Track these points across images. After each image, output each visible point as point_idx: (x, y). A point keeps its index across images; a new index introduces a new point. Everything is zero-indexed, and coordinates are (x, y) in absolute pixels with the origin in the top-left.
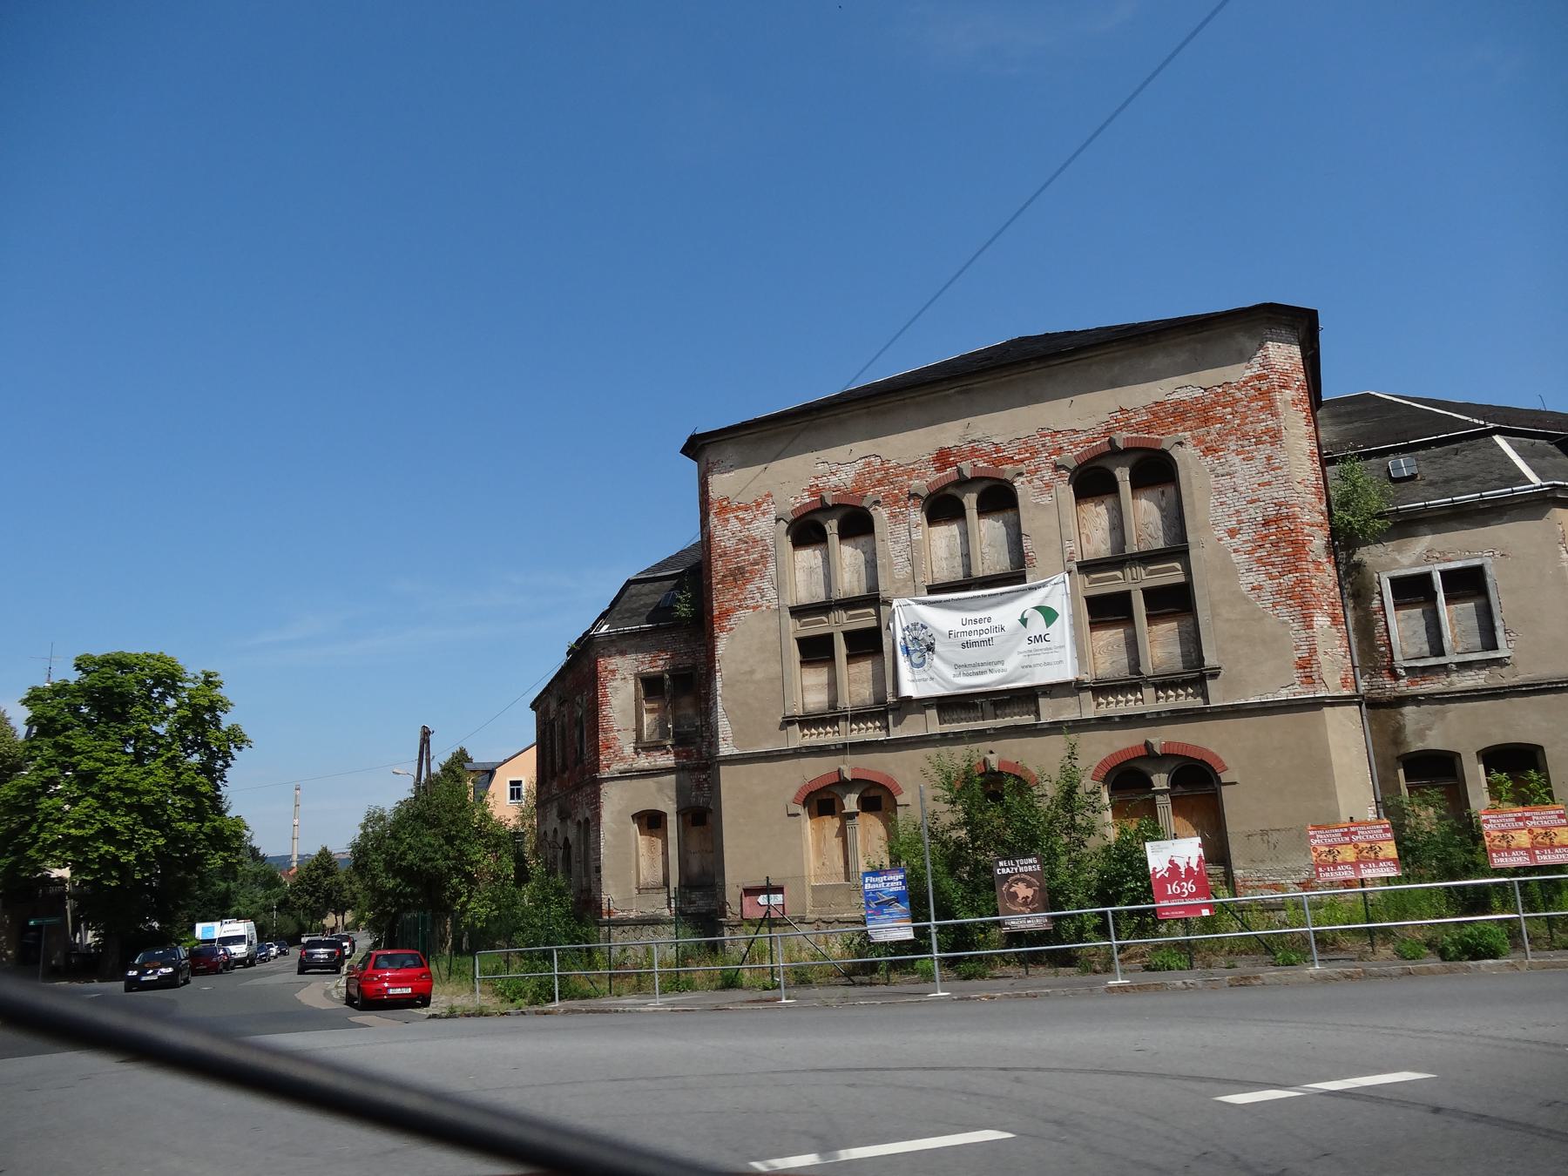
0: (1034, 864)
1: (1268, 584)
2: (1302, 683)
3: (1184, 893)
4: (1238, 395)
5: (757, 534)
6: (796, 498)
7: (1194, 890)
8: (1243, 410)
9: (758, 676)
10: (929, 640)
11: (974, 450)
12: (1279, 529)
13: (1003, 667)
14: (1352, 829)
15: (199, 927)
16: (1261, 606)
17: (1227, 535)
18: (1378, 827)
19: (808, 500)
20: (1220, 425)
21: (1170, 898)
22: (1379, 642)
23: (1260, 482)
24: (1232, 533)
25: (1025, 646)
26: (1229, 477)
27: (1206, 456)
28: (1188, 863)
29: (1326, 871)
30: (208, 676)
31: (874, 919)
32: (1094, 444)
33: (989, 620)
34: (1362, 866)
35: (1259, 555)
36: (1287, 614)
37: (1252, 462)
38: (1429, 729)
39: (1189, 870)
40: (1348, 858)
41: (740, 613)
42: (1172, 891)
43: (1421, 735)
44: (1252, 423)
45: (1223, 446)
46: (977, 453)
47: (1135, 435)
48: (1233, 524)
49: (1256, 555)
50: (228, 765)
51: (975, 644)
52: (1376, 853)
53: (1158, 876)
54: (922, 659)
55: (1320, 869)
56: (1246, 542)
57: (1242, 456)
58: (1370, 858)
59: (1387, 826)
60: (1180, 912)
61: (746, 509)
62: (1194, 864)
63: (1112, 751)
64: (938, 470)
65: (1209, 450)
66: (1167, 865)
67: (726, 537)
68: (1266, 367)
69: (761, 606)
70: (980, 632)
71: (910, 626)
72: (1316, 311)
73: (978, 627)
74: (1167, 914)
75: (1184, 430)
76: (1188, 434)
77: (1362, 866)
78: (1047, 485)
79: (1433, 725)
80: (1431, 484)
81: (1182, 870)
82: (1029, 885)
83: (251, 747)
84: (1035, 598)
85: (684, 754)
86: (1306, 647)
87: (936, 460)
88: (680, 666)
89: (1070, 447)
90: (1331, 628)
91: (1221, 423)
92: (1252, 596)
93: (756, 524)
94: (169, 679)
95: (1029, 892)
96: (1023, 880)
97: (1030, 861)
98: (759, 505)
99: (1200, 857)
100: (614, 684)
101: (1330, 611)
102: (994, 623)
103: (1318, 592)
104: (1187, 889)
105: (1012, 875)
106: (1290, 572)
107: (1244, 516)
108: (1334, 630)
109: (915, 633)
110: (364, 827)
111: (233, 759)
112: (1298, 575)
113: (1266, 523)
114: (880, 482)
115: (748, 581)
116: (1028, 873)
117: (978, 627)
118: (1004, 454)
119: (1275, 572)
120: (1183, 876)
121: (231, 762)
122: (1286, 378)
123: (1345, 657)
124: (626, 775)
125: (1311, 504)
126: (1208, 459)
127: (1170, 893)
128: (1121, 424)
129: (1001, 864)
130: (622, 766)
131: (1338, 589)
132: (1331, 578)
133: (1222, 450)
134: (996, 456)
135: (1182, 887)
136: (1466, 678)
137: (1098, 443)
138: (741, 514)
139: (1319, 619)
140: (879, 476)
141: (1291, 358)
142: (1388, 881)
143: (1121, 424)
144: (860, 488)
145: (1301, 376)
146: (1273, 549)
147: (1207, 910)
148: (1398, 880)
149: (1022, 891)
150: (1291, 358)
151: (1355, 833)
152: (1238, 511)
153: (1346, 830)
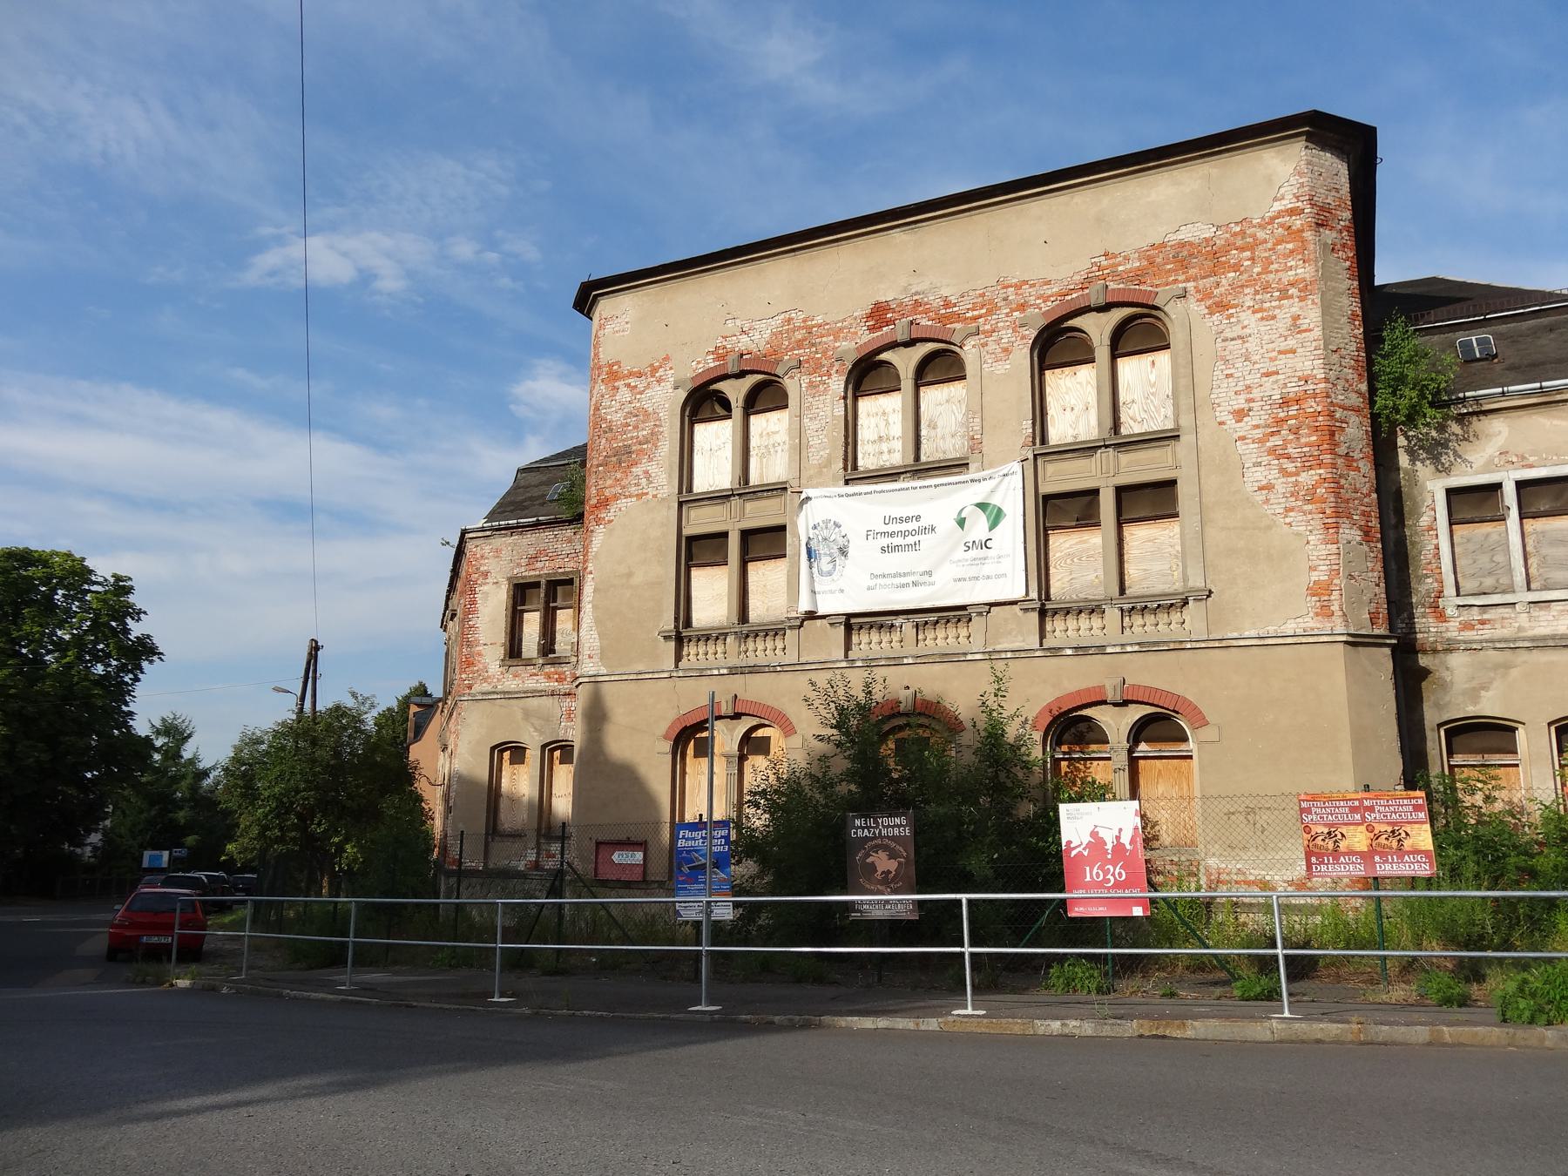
0: (901, 825)
1: (1282, 486)
2: (1317, 614)
3: (1109, 881)
4: (1261, 235)
5: (649, 406)
6: (699, 363)
7: (1124, 877)
8: (1266, 255)
9: (638, 579)
10: (841, 542)
11: (917, 303)
12: (1301, 411)
13: (931, 579)
14: (1367, 803)
15: (147, 854)
16: (1269, 512)
17: (1231, 417)
18: (1405, 802)
19: (712, 365)
20: (1233, 274)
21: (1087, 887)
22: (1425, 572)
23: (1282, 348)
24: (1240, 415)
25: (960, 553)
26: (1240, 341)
27: (1211, 314)
28: (1118, 838)
29: (1323, 863)
30: (118, 578)
31: (685, 889)
32: (1069, 298)
33: (918, 518)
34: (1377, 858)
35: (1272, 444)
36: (1304, 523)
37: (1272, 322)
38: (1484, 688)
39: (1118, 847)
40: (1357, 845)
41: (622, 503)
42: (1091, 877)
43: (1474, 695)
44: (1277, 271)
45: (1236, 302)
46: (921, 309)
47: (1122, 286)
48: (1240, 402)
49: (1268, 444)
50: (138, 680)
51: (896, 548)
52: (1399, 840)
53: (1074, 853)
54: (831, 566)
55: (1314, 860)
56: (1257, 427)
57: (1259, 315)
58: (1391, 848)
59: (1420, 801)
60: (1100, 909)
61: (639, 375)
62: (1126, 839)
63: (1058, 694)
64: (872, 329)
65: (1221, 306)
66: (1087, 839)
67: (614, 409)
68: (1301, 199)
69: (647, 494)
70: (905, 534)
71: (821, 524)
72: (1374, 130)
73: (904, 527)
74: (1081, 909)
75: (1187, 280)
76: (1190, 285)
77: (1377, 858)
78: (1006, 350)
79: (1491, 683)
80: (1511, 368)
81: (1109, 846)
82: (893, 855)
83: (162, 660)
84: (978, 493)
85: (556, 676)
86: (1325, 568)
87: (870, 316)
88: (560, 570)
89: (1038, 302)
90: (1361, 544)
91: (1235, 272)
92: (1260, 496)
93: (649, 393)
94: (78, 574)
95: (892, 865)
96: (885, 848)
97: (897, 821)
98: (654, 370)
99: (1136, 829)
100: (485, 588)
101: (1363, 523)
102: (924, 523)
103: (1347, 496)
104: (1113, 875)
105: (872, 839)
106: (1311, 468)
107: (1256, 394)
108: (1365, 548)
109: (826, 533)
110: (238, 750)
111: (142, 673)
112: (1322, 471)
113: (1285, 403)
114: (799, 344)
115: (635, 464)
116: (893, 838)
117: (904, 527)
118: (955, 309)
119: (1290, 467)
120: (1109, 856)
121: (140, 676)
122: (1328, 215)
123: (1378, 585)
124: (487, 696)
125: (1347, 381)
126: (1215, 317)
127: (1088, 879)
128: (1105, 272)
129: (857, 822)
130: (486, 687)
131: (1374, 496)
132: (1367, 480)
133: (1235, 306)
134: (944, 311)
135: (1106, 872)
136: (1542, 624)
137: (1074, 296)
138: (632, 381)
139: (1347, 531)
140: (800, 337)
141: (1337, 190)
142: (1413, 882)
143: (1105, 272)
144: (774, 355)
145: (1347, 215)
146: (1291, 437)
147: (1140, 909)
148: (1429, 883)
149: (883, 863)
150: (1337, 190)
151: (1371, 809)
152: (1248, 387)
153: (1357, 803)
